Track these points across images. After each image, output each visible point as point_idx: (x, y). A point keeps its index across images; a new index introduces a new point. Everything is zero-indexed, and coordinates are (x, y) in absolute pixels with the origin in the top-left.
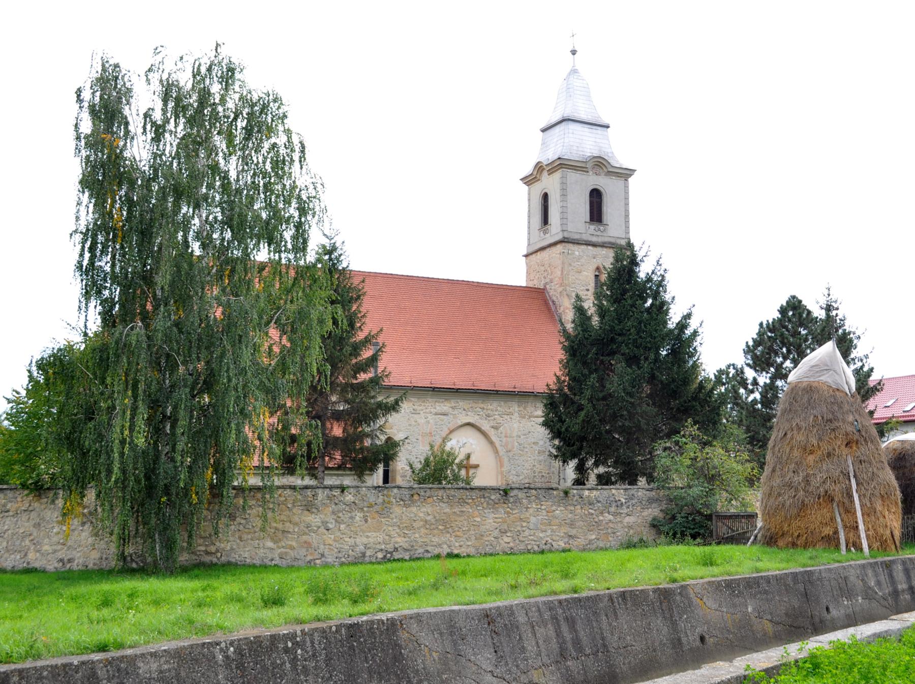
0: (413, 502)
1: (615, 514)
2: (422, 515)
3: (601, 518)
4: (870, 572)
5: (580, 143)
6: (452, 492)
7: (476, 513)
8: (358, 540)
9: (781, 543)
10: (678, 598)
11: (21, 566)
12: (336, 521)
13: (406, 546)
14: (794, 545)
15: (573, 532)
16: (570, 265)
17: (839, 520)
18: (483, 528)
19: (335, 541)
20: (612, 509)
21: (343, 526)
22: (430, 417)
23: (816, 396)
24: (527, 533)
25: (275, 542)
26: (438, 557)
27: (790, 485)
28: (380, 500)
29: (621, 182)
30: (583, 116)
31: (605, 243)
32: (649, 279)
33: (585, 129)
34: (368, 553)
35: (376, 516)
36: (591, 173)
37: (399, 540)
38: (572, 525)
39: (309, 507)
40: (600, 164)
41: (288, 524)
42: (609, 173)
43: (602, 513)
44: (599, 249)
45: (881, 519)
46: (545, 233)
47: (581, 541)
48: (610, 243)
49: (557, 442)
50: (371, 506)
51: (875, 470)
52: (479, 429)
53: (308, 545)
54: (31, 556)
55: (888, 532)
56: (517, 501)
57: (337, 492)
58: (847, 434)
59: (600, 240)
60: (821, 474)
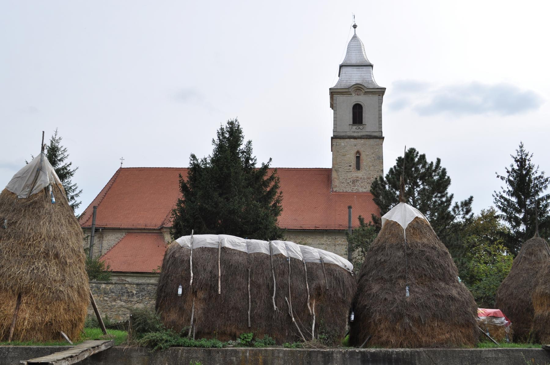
3: (114, 303)
5: (355, 77)
16: (338, 152)
20: (124, 298)
29: (376, 97)
31: (363, 136)
36: (354, 95)
42: (366, 93)
44: (359, 140)
48: (367, 135)
59: (360, 134)
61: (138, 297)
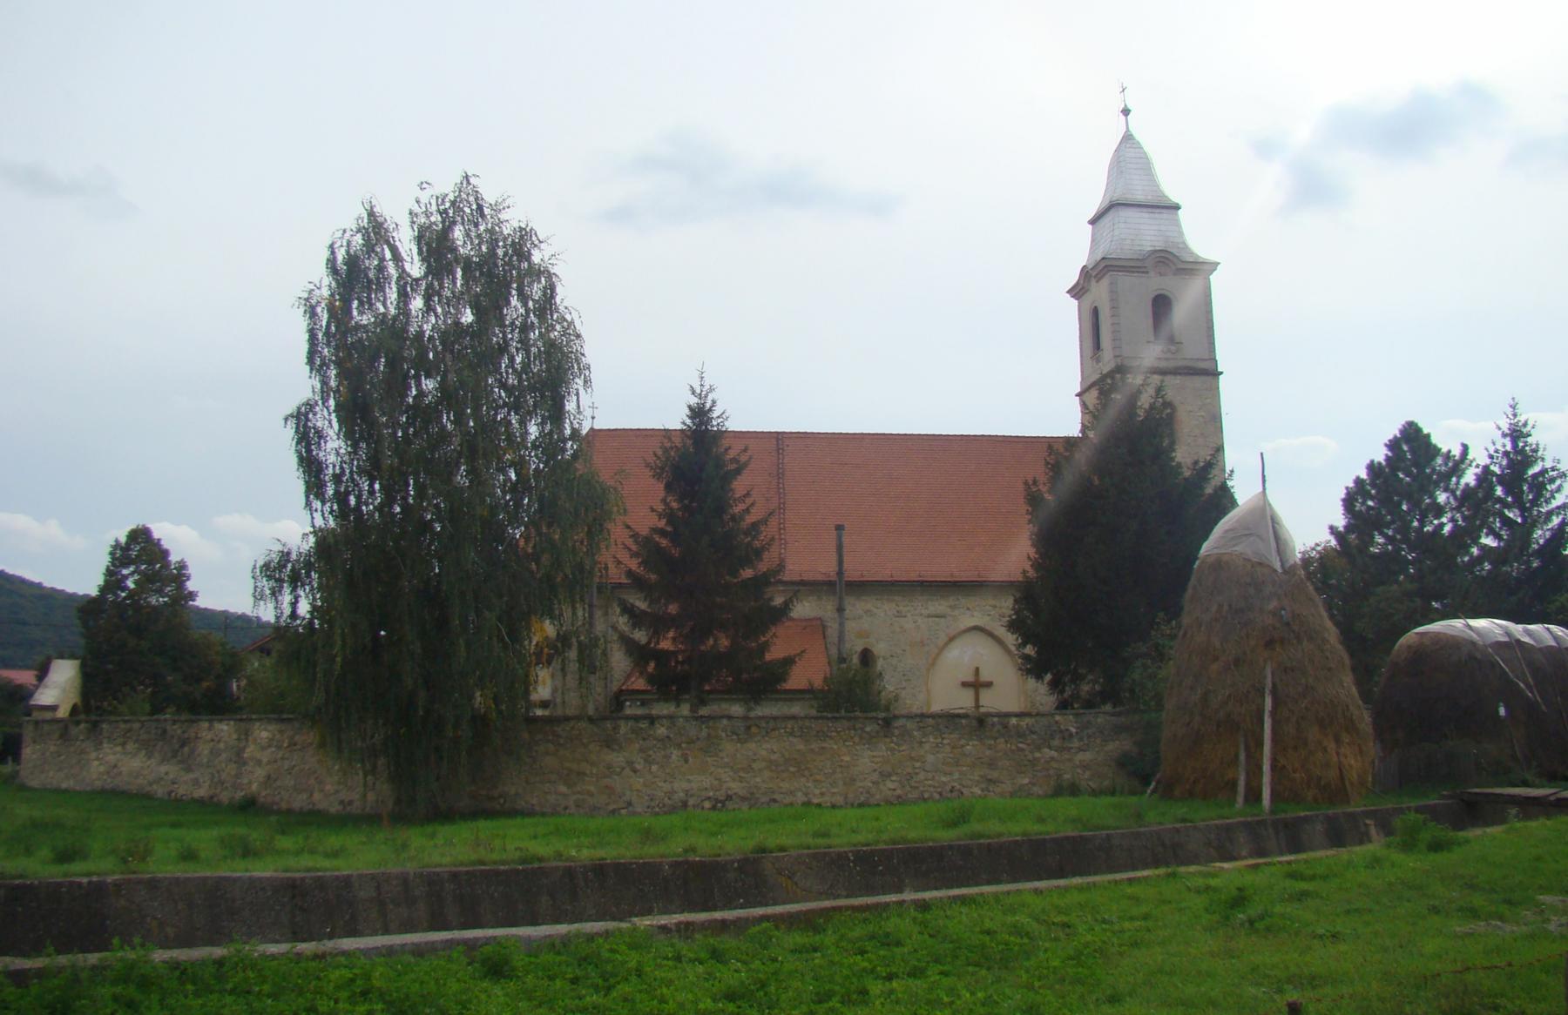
1: (1059, 749)
2: (764, 753)
3: (1037, 755)
5: (1142, 234)
6: (807, 723)
8: (676, 785)
12: (646, 760)
13: (742, 793)
14: (1191, 794)
15: (995, 775)
17: (1242, 757)
19: (645, 785)
20: (1056, 742)
21: (654, 768)
24: (922, 776)
30: (1140, 197)
34: (691, 802)
36: (1152, 274)
37: (732, 785)
38: (992, 764)
39: (609, 743)
47: (1007, 787)
57: (644, 725)
61: (1081, 739)
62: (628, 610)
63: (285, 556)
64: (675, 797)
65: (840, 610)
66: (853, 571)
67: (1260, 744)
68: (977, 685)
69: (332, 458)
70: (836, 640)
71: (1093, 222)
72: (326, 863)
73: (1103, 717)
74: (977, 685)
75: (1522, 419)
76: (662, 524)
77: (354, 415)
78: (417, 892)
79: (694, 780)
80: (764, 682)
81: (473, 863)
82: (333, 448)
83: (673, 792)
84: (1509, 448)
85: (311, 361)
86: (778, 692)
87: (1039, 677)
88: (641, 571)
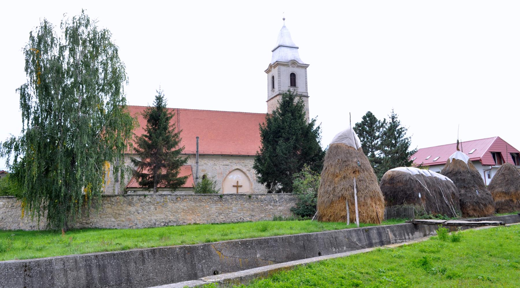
0: (178, 201)
1: (273, 206)
2: (182, 207)
4: (354, 235)
5: (286, 55)
6: (196, 197)
7: (207, 206)
8: (152, 218)
9: (324, 219)
10: (200, 251)
11: (17, 229)
13: (174, 220)
15: (254, 214)
17: (347, 208)
18: (210, 212)
20: (272, 204)
21: (145, 212)
22: (221, 166)
23: (339, 150)
24: (231, 214)
25: (116, 219)
26: (190, 224)
27: (327, 192)
28: (162, 200)
29: (303, 70)
30: (288, 44)
32: (297, 106)
33: (288, 49)
34: (157, 223)
35: (161, 207)
37: (171, 217)
38: (253, 210)
39: (130, 204)
40: (294, 63)
41: (121, 211)
42: (298, 66)
43: (267, 205)
45: (371, 208)
46: (273, 92)
47: (257, 217)
49: (260, 175)
50: (158, 203)
51: (368, 184)
52: (242, 171)
53: (130, 220)
54: (21, 224)
55: (375, 214)
56: (226, 200)
57: (142, 197)
58: (353, 168)
60: (340, 186)
62: (134, 161)
63: (13, 140)
64: (152, 222)
65: (197, 163)
66: (201, 151)
67: (353, 204)
68: (237, 186)
69: (34, 105)
70: (195, 172)
71: (273, 51)
72: (39, 254)
73: (286, 196)
74: (237, 186)
75: (395, 113)
76: (146, 133)
77: (43, 89)
78: (81, 265)
79: (158, 215)
80: (176, 185)
81: (103, 251)
82: (34, 101)
83: (151, 220)
84: (391, 121)
85: (26, 70)
86: (180, 188)
87: (262, 183)
88: (138, 148)
